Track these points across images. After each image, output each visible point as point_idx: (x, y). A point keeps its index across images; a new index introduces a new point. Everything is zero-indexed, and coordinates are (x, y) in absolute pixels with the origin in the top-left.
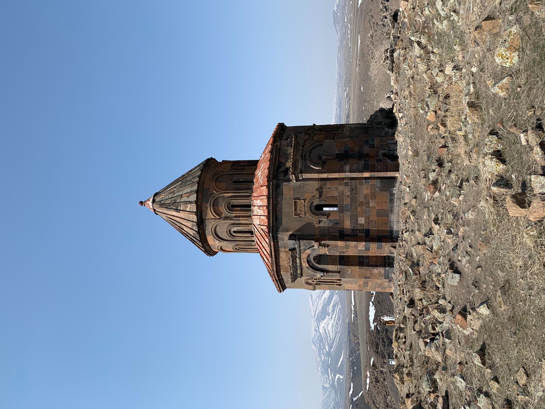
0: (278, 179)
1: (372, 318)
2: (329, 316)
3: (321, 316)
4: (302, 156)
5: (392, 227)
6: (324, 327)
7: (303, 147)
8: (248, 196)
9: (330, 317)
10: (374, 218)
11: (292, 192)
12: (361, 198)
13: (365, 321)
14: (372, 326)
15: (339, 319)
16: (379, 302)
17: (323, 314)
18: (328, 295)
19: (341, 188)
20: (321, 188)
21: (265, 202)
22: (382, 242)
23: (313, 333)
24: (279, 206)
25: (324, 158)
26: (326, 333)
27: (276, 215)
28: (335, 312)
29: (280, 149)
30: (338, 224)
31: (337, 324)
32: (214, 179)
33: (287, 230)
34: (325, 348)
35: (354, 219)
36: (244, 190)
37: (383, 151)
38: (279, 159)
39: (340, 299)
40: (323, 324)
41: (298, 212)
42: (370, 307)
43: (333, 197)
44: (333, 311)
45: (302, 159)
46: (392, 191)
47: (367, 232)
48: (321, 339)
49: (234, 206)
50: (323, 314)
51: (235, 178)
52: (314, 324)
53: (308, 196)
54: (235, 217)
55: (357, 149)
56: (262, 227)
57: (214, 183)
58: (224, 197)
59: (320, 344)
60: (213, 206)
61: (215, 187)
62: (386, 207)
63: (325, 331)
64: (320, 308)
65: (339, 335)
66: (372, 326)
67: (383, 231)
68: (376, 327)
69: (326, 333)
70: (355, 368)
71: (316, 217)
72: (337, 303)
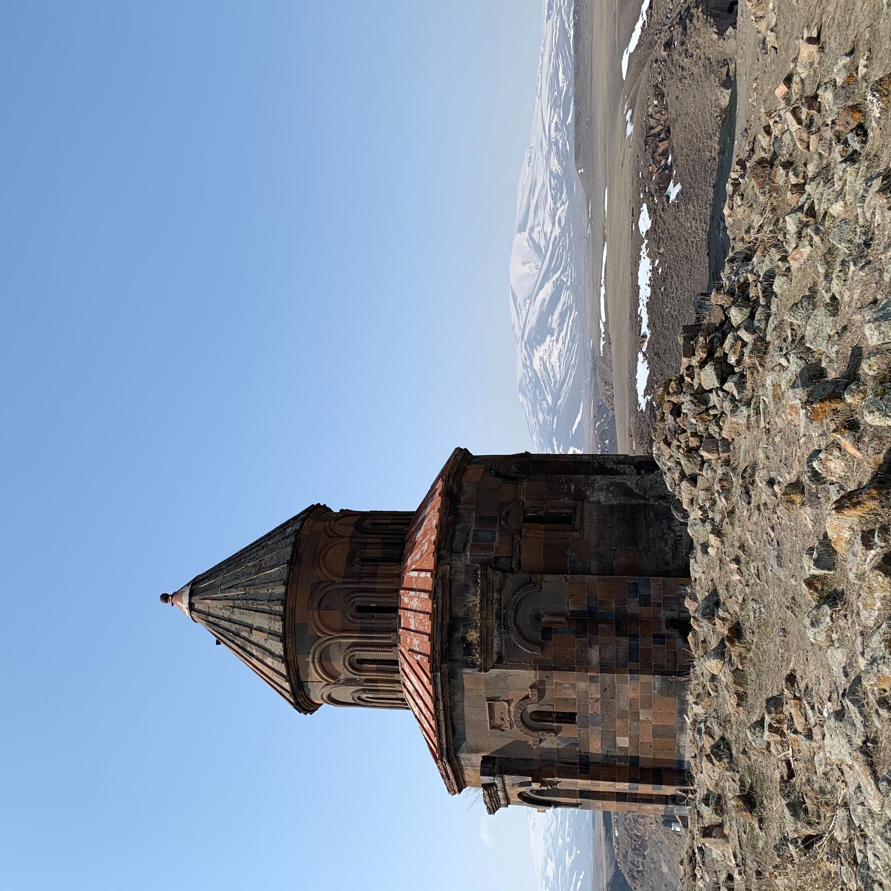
0: (452, 661)
2: (552, 335)
3: (536, 336)
4: (498, 617)
5: (684, 756)
6: (541, 359)
7: (500, 591)
9: (554, 338)
11: (482, 686)
13: (627, 392)
14: (643, 402)
15: (572, 340)
16: (657, 354)
17: (541, 331)
18: (550, 291)
19: (582, 685)
21: (426, 625)
23: (520, 371)
24: (458, 710)
25: (545, 619)
26: (546, 369)
27: (453, 724)
28: (565, 326)
29: (451, 581)
30: (577, 745)
32: (315, 605)
33: (476, 751)
34: (545, 399)
35: (609, 737)
36: (380, 632)
37: (669, 614)
38: (450, 608)
39: (576, 300)
40: (539, 352)
41: (498, 722)
42: (639, 363)
43: (567, 699)
44: (561, 325)
45: (499, 625)
46: (684, 697)
48: (536, 383)
49: (362, 661)
50: (541, 331)
51: (359, 601)
52: (521, 354)
53: (516, 696)
54: (367, 681)
56: (419, 657)
57: (316, 613)
58: (340, 644)
60: (320, 661)
61: (319, 624)
62: (671, 722)
63: (545, 366)
64: (533, 320)
65: (573, 372)
66: (643, 402)
67: (665, 761)
68: (649, 404)
69: (546, 369)
70: (607, 442)
72: (570, 308)
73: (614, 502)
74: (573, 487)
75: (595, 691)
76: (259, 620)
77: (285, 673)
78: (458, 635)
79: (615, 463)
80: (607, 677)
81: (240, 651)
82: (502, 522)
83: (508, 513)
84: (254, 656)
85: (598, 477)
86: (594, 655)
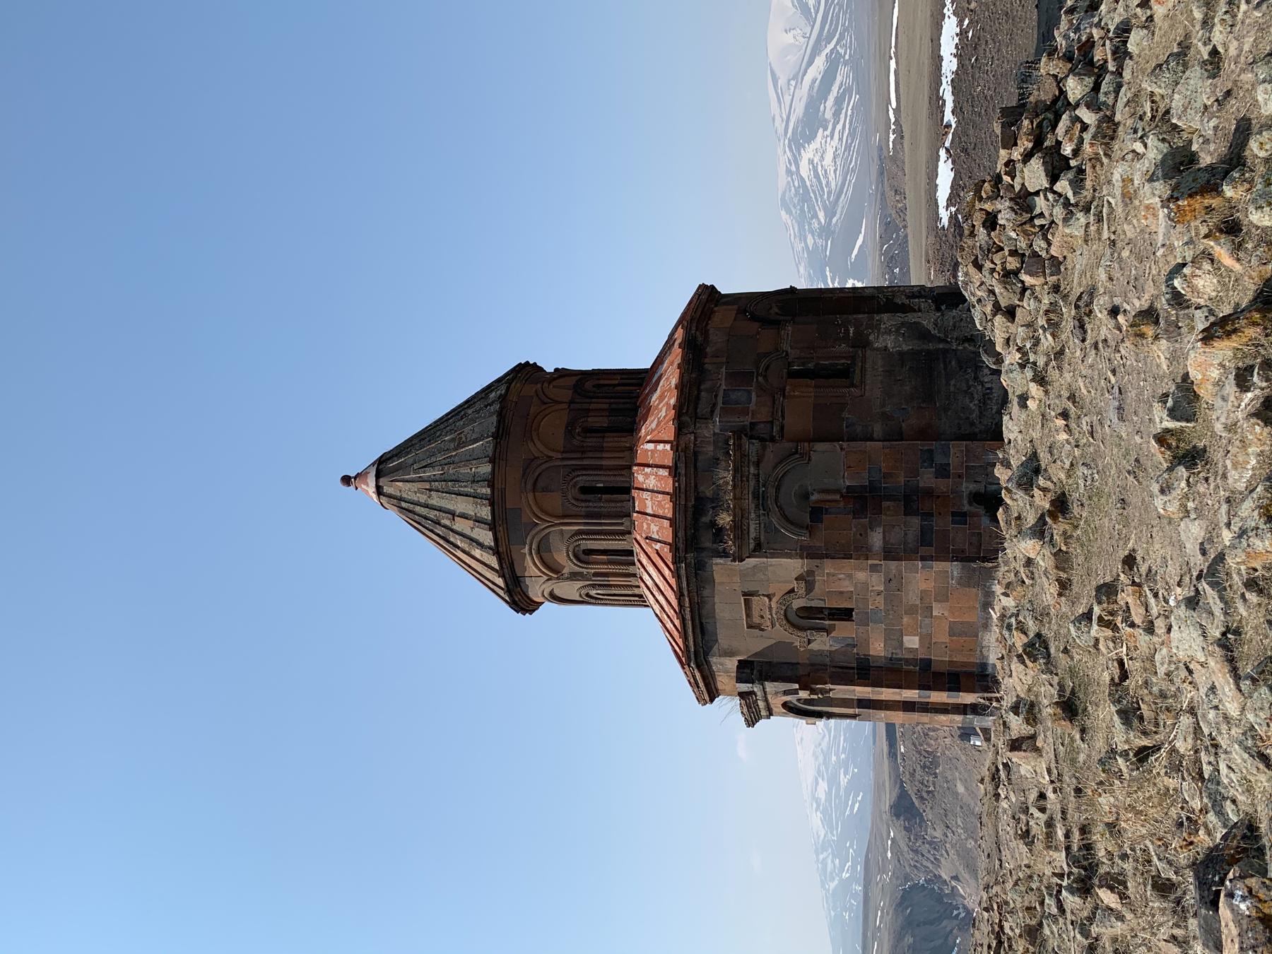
1: (943, 193)
2: (825, 129)
4: (756, 496)
6: (811, 162)
7: (757, 464)
8: (623, 533)
9: (828, 132)
10: (942, 637)
12: (912, 598)
13: (924, 202)
14: (944, 215)
15: (852, 134)
16: (965, 150)
18: (822, 68)
19: (861, 576)
20: (810, 573)
22: (959, 691)
23: (783, 180)
26: (817, 176)
27: (701, 624)
28: (842, 116)
29: (696, 454)
31: (848, 147)
32: (529, 486)
33: (730, 653)
34: (815, 216)
35: (895, 636)
37: (973, 487)
38: (696, 486)
40: (808, 153)
41: (756, 620)
42: (941, 164)
43: (842, 593)
44: (837, 114)
45: (757, 507)
46: (990, 587)
47: (926, 664)
48: (804, 195)
51: (583, 480)
52: (784, 157)
53: (779, 589)
54: (596, 574)
55: (902, 479)
56: (658, 546)
57: (530, 496)
59: (802, 210)
60: (538, 552)
62: (973, 617)
66: (944, 215)
67: (965, 664)
68: (953, 218)
69: (817, 176)
71: (803, 634)
73: (905, 348)
74: (851, 330)
75: (877, 582)
76: (461, 505)
77: (497, 567)
78: (706, 519)
79: (908, 297)
80: (893, 565)
81: (442, 542)
82: (760, 379)
83: (767, 368)
84: (458, 547)
85: (885, 316)
86: (876, 539)
